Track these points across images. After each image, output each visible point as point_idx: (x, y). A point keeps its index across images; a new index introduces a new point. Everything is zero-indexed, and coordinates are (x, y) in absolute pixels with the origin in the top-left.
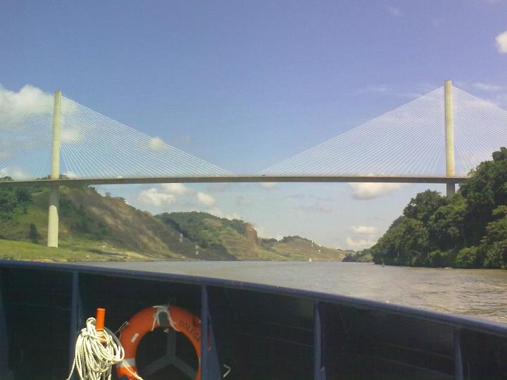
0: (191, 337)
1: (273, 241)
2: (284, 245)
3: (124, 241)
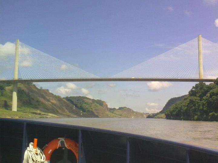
0: (74, 152)
1: (114, 109)
2: (119, 110)
3: (48, 110)
